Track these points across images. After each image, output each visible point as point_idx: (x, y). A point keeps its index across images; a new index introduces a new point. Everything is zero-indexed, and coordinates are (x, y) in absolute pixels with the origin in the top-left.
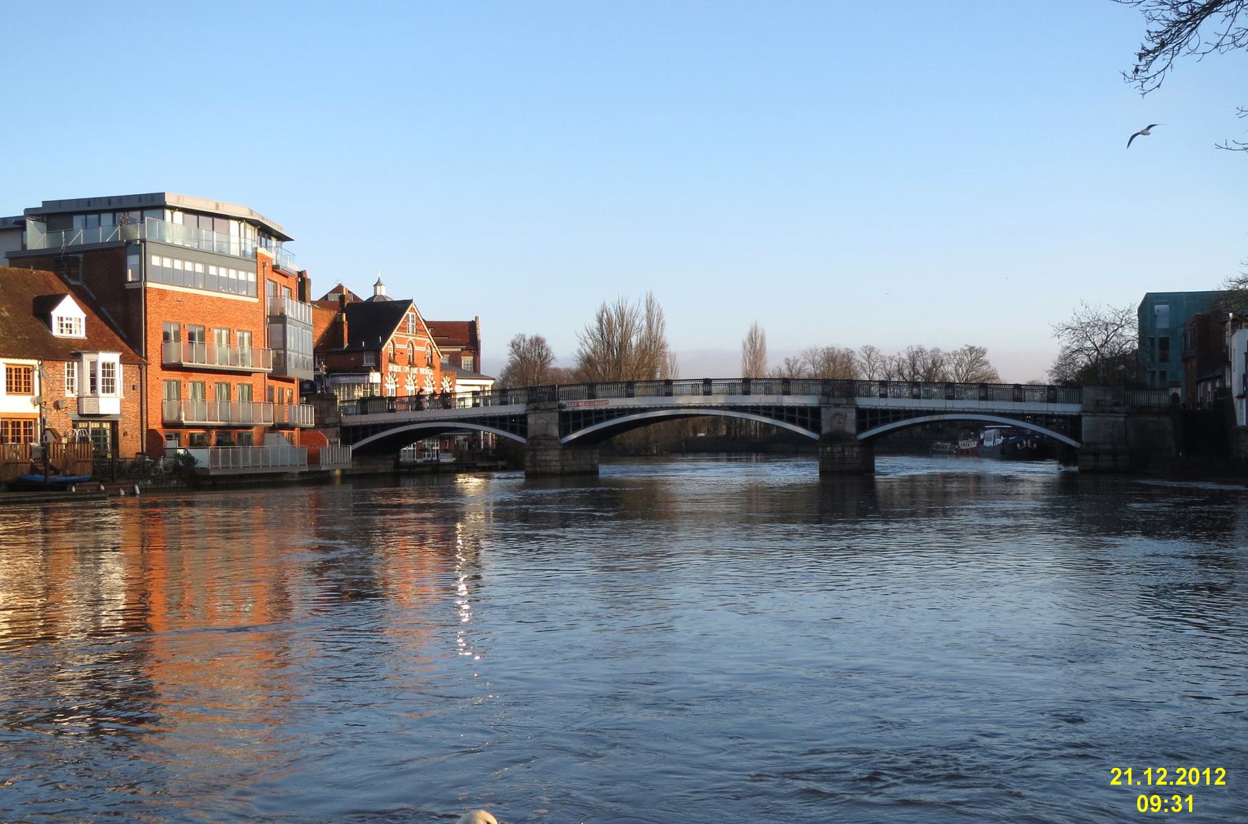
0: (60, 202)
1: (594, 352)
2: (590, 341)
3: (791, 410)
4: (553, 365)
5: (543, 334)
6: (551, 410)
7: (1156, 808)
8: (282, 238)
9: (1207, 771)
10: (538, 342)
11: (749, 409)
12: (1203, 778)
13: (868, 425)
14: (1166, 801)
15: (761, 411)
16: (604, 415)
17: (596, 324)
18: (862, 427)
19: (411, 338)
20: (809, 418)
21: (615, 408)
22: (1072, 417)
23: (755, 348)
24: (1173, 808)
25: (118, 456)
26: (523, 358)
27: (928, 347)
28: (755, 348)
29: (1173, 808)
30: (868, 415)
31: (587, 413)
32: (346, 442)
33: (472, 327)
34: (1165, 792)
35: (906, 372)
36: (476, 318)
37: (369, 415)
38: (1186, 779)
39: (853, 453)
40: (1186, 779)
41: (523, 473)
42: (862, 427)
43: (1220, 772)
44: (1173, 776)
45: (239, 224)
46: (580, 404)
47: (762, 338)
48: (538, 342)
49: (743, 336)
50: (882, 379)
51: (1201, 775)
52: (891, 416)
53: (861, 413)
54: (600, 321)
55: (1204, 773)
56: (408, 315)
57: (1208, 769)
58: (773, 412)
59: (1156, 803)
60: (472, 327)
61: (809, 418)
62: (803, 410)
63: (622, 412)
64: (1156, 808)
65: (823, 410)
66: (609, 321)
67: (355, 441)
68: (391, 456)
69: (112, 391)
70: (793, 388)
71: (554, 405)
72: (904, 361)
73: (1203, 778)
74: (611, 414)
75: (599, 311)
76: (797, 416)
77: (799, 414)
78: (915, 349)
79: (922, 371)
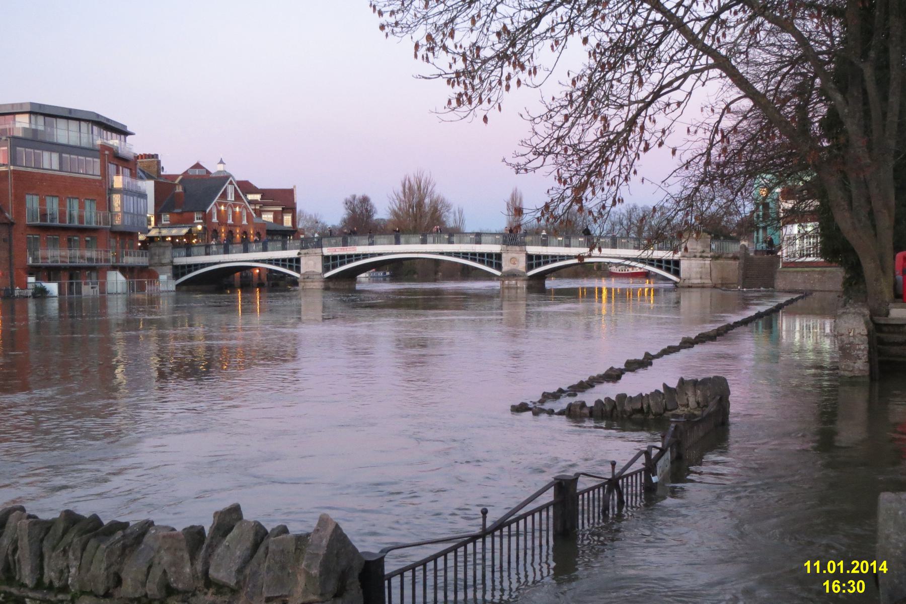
0: (108, 120)
1: (400, 209)
2: (397, 202)
3: (482, 255)
4: (376, 217)
5: (369, 195)
7: (836, 583)
8: (122, 132)
9: (874, 563)
10: (365, 200)
12: (871, 568)
14: (844, 585)
15: (469, 256)
16: (354, 258)
17: (401, 189)
18: (530, 267)
20: (494, 261)
24: (849, 590)
25: (108, 270)
26: (353, 211)
27: (640, 205)
29: (849, 590)
31: (342, 257)
32: (176, 276)
33: (290, 193)
34: (843, 578)
35: (625, 222)
36: (295, 187)
38: (859, 569)
40: (859, 569)
42: (530, 267)
43: (855, 564)
44: (848, 566)
47: (521, 199)
48: (365, 200)
49: (508, 197)
51: (869, 565)
52: (550, 259)
53: (530, 257)
54: (404, 186)
55: (871, 565)
56: (226, 190)
57: (809, 562)
59: (836, 587)
60: (290, 193)
61: (494, 261)
62: (490, 255)
63: (365, 256)
64: (836, 583)
65: (504, 255)
66: (410, 188)
70: (483, 238)
71: (318, 250)
72: (624, 215)
73: (871, 568)
74: (358, 257)
75: (403, 179)
76: (486, 259)
77: (487, 257)
78: (631, 206)
79: (636, 222)
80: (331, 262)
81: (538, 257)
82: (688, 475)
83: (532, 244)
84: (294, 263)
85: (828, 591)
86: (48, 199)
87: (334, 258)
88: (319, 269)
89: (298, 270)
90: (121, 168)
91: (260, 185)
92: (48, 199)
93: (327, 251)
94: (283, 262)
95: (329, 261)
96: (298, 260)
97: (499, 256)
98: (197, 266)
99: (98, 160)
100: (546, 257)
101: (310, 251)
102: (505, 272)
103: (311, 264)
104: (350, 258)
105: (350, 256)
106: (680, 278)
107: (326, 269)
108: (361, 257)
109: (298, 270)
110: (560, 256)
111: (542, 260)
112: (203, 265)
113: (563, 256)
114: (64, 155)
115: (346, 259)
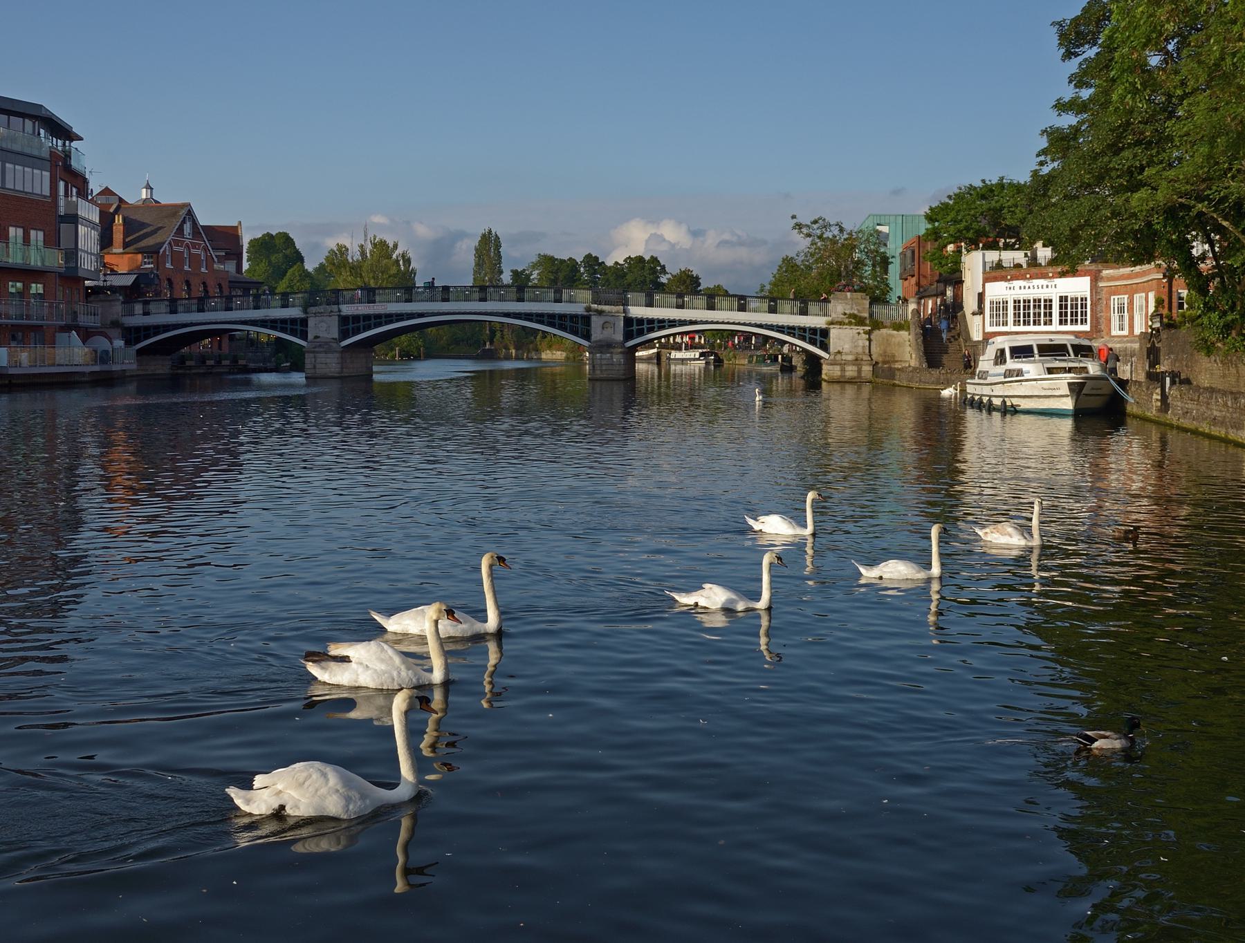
6: (330, 314)
11: (523, 316)
13: (351, 332)
19: (187, 241)
21: (775, 324)
22: (583, 317)
23: (489, 246)
28: (489, 246)
30: (351, 321)
31: (367, 317)
37: (206, 313)
39: (618, 358)
41: (303, 375)
44: (1004, 402)
45: (34, 123)
46: (360, 308)
50: (867, 302)
52: (656, 325)
53: (344, 320)
58: (545, 319)
60: (107, 189)
63: (400, 317)
67: (138, 341)
68: (169, 357)
69: (1007, 325)
71: (335, 308)
74: (390, 318)
76: (557, 321)
80: (362, 322)
82: (1076, 131)
84: (298, 326)
85: (968, 381)
86: (33, 233)
87: (356, 318)
88: (335, 333)
89: (304, 336)
90: (62, 184)
92: (33, 233)
93: (347, 310)
94: (801, 332)
95: (359, 322)
96: (304, 322)
97: (825, 333)
98: (158, 329)
99: (47, 174)
100: (651, 321)
101: (321, 309)
102: (596, 342)
103: (323, 327)
104: (380, 319)
105: (378, 316)
106: (829, 353)
107: (344, 334)
108: (395, 318)
109: (304, 336)
110: (670, 321)
111: (645, 326)
112: (167, 328)
113: (674, 321)
114: (7, 165)
115: (373, 321)
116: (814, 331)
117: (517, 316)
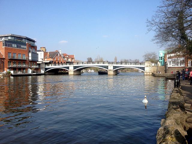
8: (34, 41)
42: (114, 69)
48: (91, 58)
53: (114, 67)
74: (80, 67)
81: (115, 67)
83: (114, 64)
89: (108, 68)
91: (68, 54)
98: (49, 68)
104: (79, 67)
116: (142, 67)
117: (98, 66)
